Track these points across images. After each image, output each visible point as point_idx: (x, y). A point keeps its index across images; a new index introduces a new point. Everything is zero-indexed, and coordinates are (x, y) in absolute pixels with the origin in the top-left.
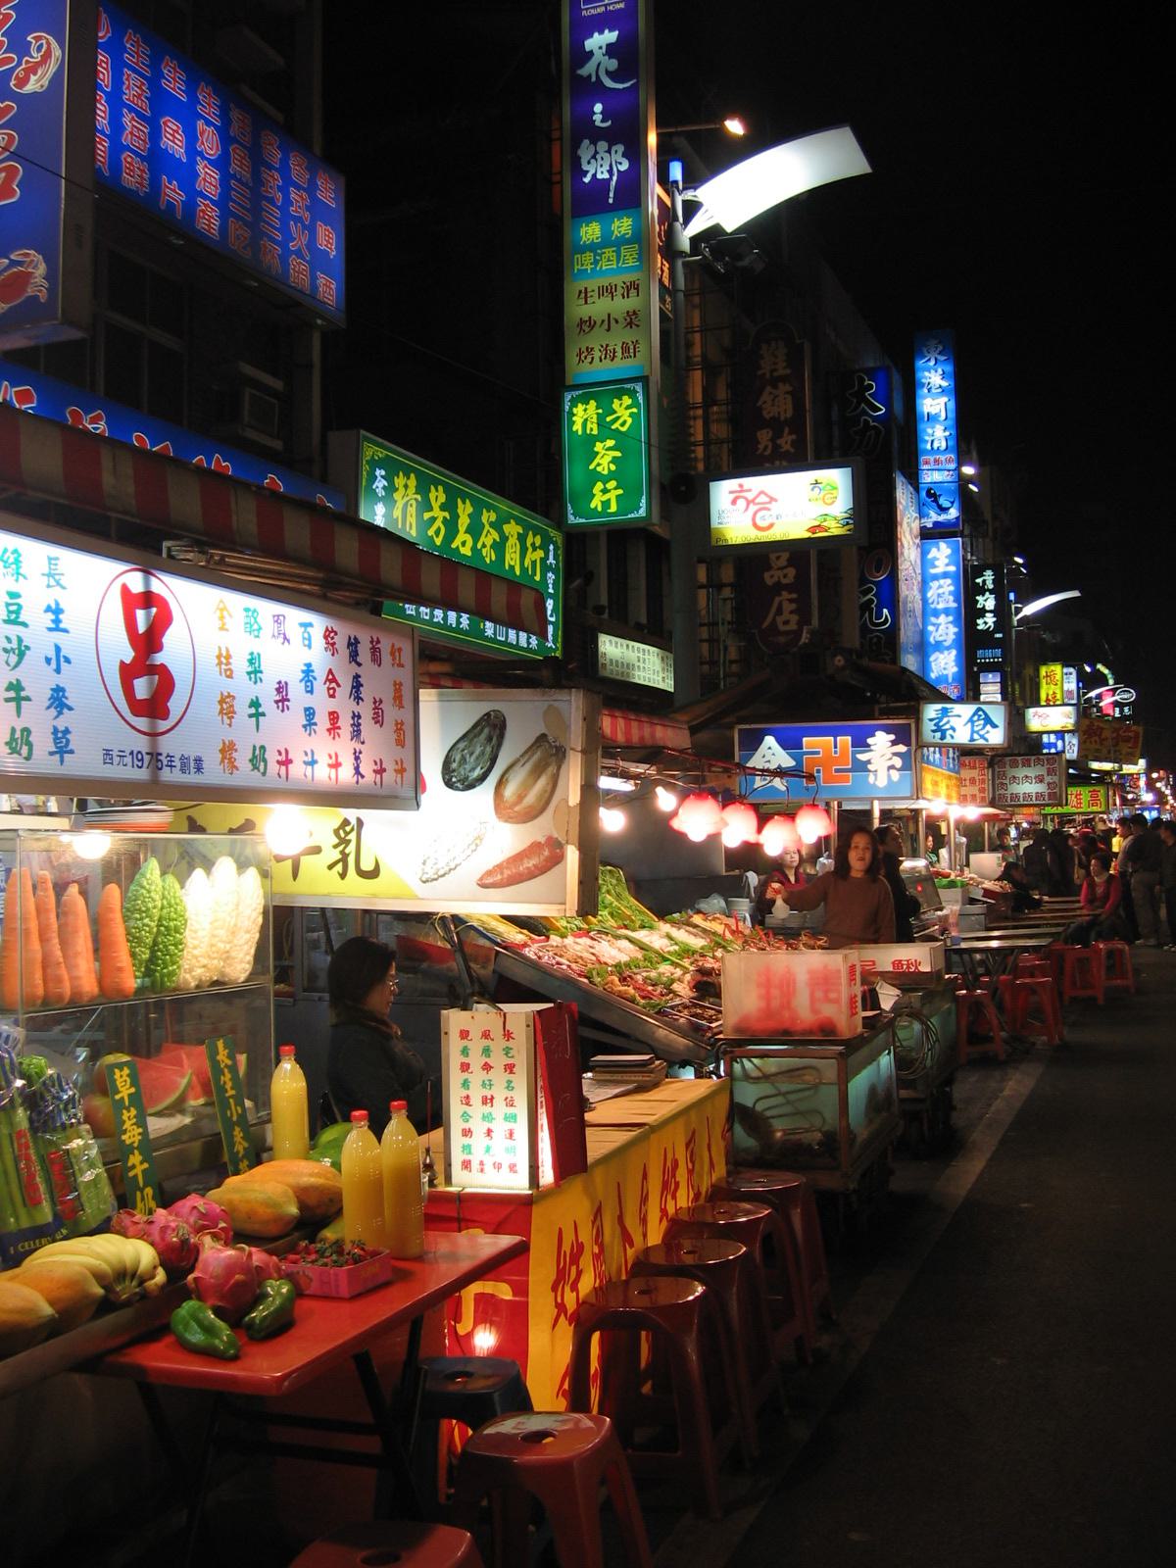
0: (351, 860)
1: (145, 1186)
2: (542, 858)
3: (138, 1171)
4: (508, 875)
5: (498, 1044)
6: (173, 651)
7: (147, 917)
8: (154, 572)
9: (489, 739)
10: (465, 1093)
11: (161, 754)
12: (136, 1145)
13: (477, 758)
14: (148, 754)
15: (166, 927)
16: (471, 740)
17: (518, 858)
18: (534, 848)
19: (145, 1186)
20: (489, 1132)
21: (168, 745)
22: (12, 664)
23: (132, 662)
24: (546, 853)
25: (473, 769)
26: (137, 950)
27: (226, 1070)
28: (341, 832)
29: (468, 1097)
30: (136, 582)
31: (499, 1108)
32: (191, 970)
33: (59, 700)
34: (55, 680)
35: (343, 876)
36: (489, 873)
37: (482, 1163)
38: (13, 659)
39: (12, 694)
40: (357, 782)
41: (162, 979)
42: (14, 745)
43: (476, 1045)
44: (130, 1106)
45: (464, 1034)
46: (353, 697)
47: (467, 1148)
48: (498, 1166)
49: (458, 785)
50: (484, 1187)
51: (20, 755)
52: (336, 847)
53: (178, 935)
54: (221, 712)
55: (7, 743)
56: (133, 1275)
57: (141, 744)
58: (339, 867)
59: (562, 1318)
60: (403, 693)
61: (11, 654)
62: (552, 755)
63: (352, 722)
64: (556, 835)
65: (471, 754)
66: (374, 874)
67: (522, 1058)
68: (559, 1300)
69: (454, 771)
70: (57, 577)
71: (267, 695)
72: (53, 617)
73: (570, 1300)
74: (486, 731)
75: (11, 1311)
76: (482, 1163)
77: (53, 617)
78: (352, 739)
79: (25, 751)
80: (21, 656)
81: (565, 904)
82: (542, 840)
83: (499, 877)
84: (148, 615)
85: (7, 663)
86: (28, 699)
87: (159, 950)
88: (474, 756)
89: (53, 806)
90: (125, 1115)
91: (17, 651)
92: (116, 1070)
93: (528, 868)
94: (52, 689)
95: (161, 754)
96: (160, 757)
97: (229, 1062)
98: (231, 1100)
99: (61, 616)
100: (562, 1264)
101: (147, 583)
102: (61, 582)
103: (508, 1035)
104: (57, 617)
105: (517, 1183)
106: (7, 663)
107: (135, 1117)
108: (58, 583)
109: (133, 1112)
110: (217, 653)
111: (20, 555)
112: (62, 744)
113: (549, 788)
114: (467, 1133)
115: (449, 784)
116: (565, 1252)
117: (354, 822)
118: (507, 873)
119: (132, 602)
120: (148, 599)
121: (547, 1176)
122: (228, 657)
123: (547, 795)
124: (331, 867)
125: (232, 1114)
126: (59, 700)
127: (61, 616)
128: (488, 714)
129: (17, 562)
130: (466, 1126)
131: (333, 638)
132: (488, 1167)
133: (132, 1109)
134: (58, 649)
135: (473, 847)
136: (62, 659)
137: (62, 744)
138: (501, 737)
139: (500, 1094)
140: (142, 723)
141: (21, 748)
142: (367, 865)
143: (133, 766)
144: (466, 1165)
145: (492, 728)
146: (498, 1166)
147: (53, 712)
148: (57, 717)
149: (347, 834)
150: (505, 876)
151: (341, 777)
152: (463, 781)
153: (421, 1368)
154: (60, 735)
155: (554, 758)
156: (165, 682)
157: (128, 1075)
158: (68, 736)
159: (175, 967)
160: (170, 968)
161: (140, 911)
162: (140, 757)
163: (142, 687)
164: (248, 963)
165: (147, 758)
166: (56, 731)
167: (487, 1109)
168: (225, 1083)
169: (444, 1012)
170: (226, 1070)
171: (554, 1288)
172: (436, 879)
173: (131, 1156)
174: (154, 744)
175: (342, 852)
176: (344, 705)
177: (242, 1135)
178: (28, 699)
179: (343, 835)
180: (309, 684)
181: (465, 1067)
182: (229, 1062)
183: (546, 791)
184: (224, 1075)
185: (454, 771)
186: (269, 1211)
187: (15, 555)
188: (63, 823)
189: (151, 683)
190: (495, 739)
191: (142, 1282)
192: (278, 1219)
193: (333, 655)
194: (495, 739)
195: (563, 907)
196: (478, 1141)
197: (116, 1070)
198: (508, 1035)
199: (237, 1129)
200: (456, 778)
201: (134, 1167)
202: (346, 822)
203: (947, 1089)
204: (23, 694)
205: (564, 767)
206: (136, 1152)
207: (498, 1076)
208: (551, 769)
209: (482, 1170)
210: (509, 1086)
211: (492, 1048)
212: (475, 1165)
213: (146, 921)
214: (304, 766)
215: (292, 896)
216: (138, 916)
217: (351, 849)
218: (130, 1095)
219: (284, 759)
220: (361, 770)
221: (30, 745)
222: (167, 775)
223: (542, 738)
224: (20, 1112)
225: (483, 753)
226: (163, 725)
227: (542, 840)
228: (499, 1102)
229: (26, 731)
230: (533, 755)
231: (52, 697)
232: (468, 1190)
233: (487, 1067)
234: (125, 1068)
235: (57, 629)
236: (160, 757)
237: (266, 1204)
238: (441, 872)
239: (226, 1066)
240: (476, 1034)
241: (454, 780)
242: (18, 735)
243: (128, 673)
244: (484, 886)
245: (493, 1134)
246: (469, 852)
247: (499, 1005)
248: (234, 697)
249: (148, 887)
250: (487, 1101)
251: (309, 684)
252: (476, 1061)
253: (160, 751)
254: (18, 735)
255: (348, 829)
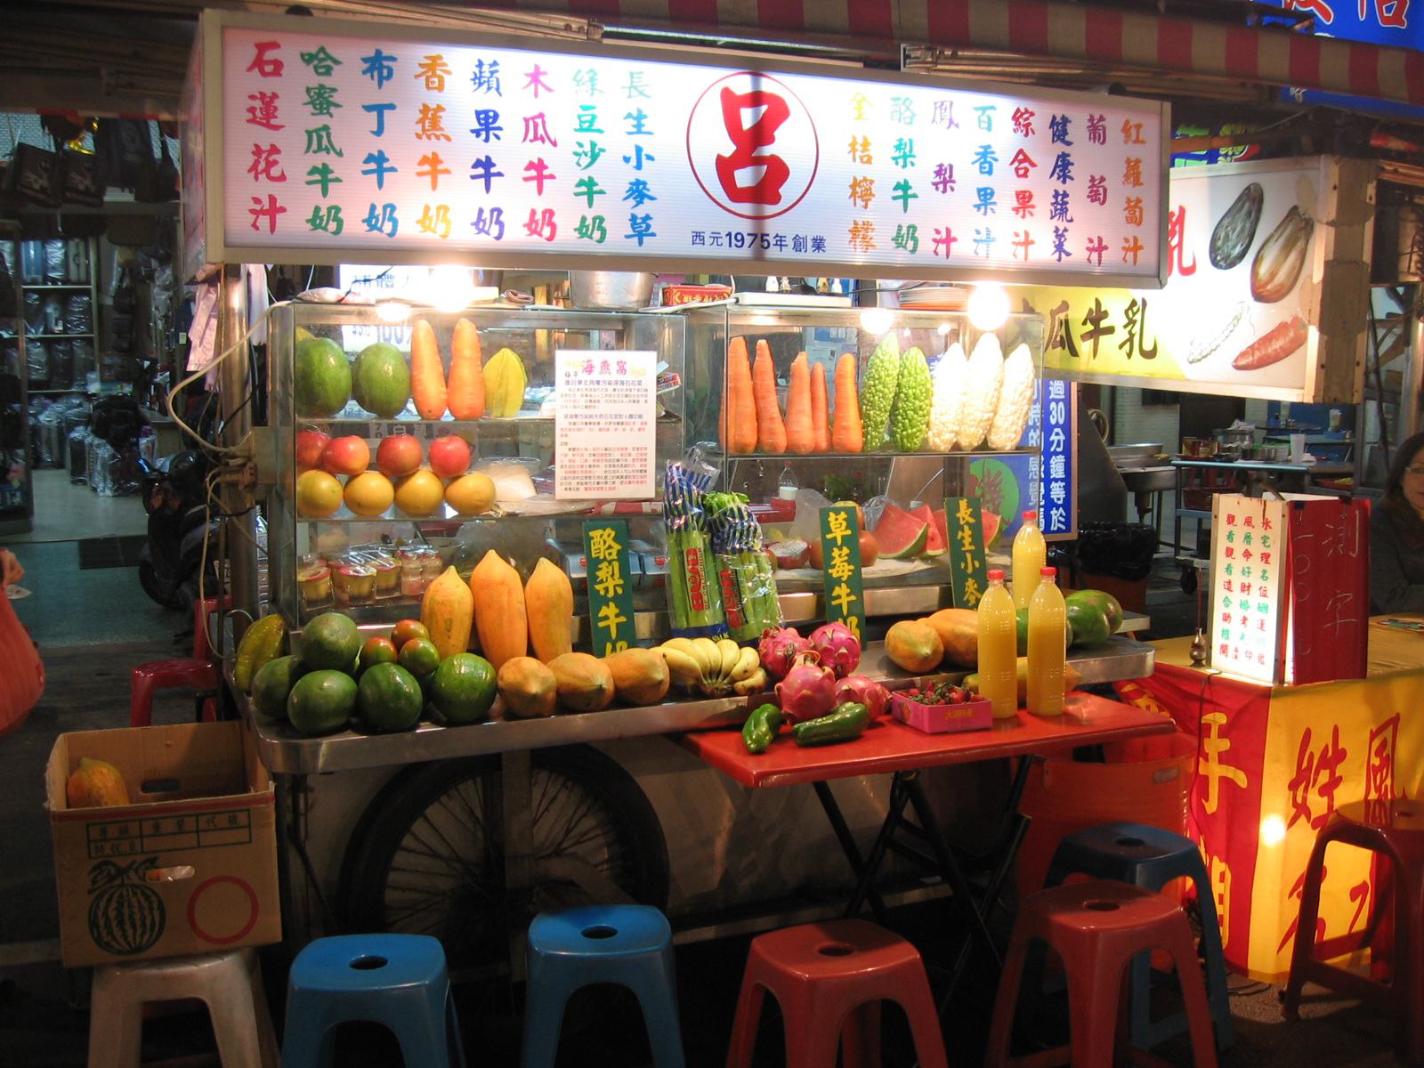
0: (1136, 339)
1: (849, 614)
2: (1288, 339)
3: (844, 601)
4: (1258, 358)
5: (1257, 532)
6: (786, 144)
7: (880, 383)
8: (765, 73)
9: (1249, 214)
10: (1227, 578)
11: (768, 235)
12: (844, 579)
13: (1238, 235)
14: (749, 235)
15: (906, 394)
16: (1234, 216)
17: (1267, 339)
18: (1282, 328)
19: (849, 614)
20: (1245, 619)
21: (772, 228)
22: (584, 165)
23: (731, 156)
24: (1291, 334)
25: (1234, 247)
26: (872, 413)
27: (966, 528)
28: (1130, 312)
29: (1229, 582)
30: (742, 84)
31: (1254, 597)
32: (939, 435)
33: (638, 192)
34: (635, 175)
35: (1129, 355)
36: (1243, 355)
37: (1236, 650)
38: (585, 161)
39: (900, 193)
40: (1059, 260)
41: (902, 439)
42: (534, 226)
43: (1240, 530)
44: (842, 545)
45: (1231, 519)
46: (1056, 176)
47: (1225, 633)
48: (1249, 655)
49: (1222, 263)
50: (1236, 673)
51: (540, 235)
52: (1125, 327)
53: (917, 402)
54: (853, 194)
55: (525, 225)
56: (727, 675)
57: (745, 227)
58: (1127, 347)
59: (1303, 819)
60: (1141, 169)
61: (583, 156)
62: (1301, 229)
63: (1054, 200)
64: (1300, 315)
65: (1234, 232)
66: (1150, 355)
67: (1276, 549)
68: (1299, 800)
69: (1219, 249)
70: (640, 89)
71: (918, 180)
72: (635, 122)
73: (1318, 804)
74: (1247, 205)
75: (580, 678)
76: (1236, 650)
77: (635, 122)
78: (1052, 218)
79: (910, 244)
80: (594, 157)
81: (1302, 388)
82: (1289, 320)
83: (1251, 359)
84: (756, 115)
85: (578, 164)
86: (915, 196)
87: (899, 414)
88: (1236, 232)
89: (837, 287)
90: (836, 552)
91: (589, 154)
92: (831, 514)
93: (1276, 350)
94: (631, 183)
95: (768, 235)
96: (766, 238)
97: (972, 520)
98: (968, 555)
99: (643, 121)
100: (1305, 764)
101: (756, 84)
102: (645, 92)
103: (1266, 524)
104: (639, 122)
105: (1263, 676)
106: (578, 164)
107: (847, 555)
108: (641, 93)
109: (846, 550)
110: (850, 141)
111: (595, 74)
112: (641, 228)
113: (1298, 265)
114: (1227, 618)
115: (1215, 263)
116: (1312, 755)
117: (1140, 303)
118: (1257, 354)
119: (731, 104)
120: (756, 99)
121: (1289, 676)
122: (866, 144)
123: (1295, 272)
124: (1121, 347)
125: (966, 567)
126: (638, 192)
127: (643, 121)
128: (1248, 188)
129: (592, 79)
130: (1227, 611)
131: (1027, 119)
132: (1241, 655)
133: (844, 548)
134: (639, 150)
135: (1231, 328)
136: (644, 157)
137: (641, 228)
138: (1259, 211)
139: (1255, 581)
140: (745, 208)
141: (542, 228)
142: (1148, 347)
143: (730, 246)
144: (1224, 649)
145: (1252, 201)
146: (1249, 655)
147: (632, 202)
148: (636, 205)
149: (1134, 314)
150: (1256, 358)
151: (1031, 257)
152: (1225, 259)
153: (1023, 817)
154: (639, 221)
155: (1303, 232)
156: (777, 172)
157: (845, 519)
158: (649, 222)
159: (915, 430)
160: (910, 431)
161: (874, 379)
162: (739, 237)
163: (744, 177)
164: (1015, 432)
165: (748, 240)
166: (634, 218)
167: (1244, 596)
168: (963, 538)
169: (1216, 495)
170: (966, 528)
171: (1293, 786)
172: (1199, 360)
173: (837, 588)
174: (760, 227)
175: (1130, 332)
176: (1042, 184)
177: (976, 586)
178: (915, 196)
179: (1131, 315)
180: (987, 165)
181: (1229, 552)
182: (972, 520)
183: (1294, 268)
184: (963, 531)
185: (1219, 249)
186: (906, 648)
187: (591, 74)
188: (848, 301)
189: (757, 173)
190: (1253, 214)
191: (733, 681)
192: (912, 656)
193: (1027, 135)
194: (1253, 214)
195: (1302, 391)
196: (1235, 625)
197: (831, 514)
198: (1266, 524)
199: (970, 582)
200: (1222, 258)
201: (839, 597)
202: (1134, 303)
203: (808, 563)
204: (910, 192)
205: (1311, 241)
206: (843, 585)
207: (1255, 563)
208: (1300, 245)
209: (1236, 657)
210: (1264, 576)
211: (1252, 535)
212: (1231, 651)
213: (880, 387)
214: (1014, 247)
215: (1092, 374)
216: (872, 383)
217: (1136, 329)
218: (843, 537)
219: (1096, 246)
220: (1067, 247)
221: (553, 226)
222: (773, 253)
223: (1294, 209)
224: (695, 534)
225: (1243, 229)
226: (770, 209)
227: (1289, 320)
228: (1255, 591)
229: (912, 228)
230: (1285, 230)
231: (631, 189)
232: (1224, 675)
233: (1247, 554)
234: (842, 513)
235: (639, 132)
236: (766, 238)
237: (905, 642)
238: (1204, 354)
239: (967, 523)
240: (1240, 520)
241: (1219, 258)
242: (904, 231)
243: (725, 168)
244: (1238, 368)
245: (1247, 622)
246: (1227, 333)
247: (1282, 494)
248: (872, 182)
249: (882, 357)
250: (1245, 588)
251: (987, 165)
252: (1239, 547)
253: (767, 232)
254: (904, 231)
255: (1135, 309)
